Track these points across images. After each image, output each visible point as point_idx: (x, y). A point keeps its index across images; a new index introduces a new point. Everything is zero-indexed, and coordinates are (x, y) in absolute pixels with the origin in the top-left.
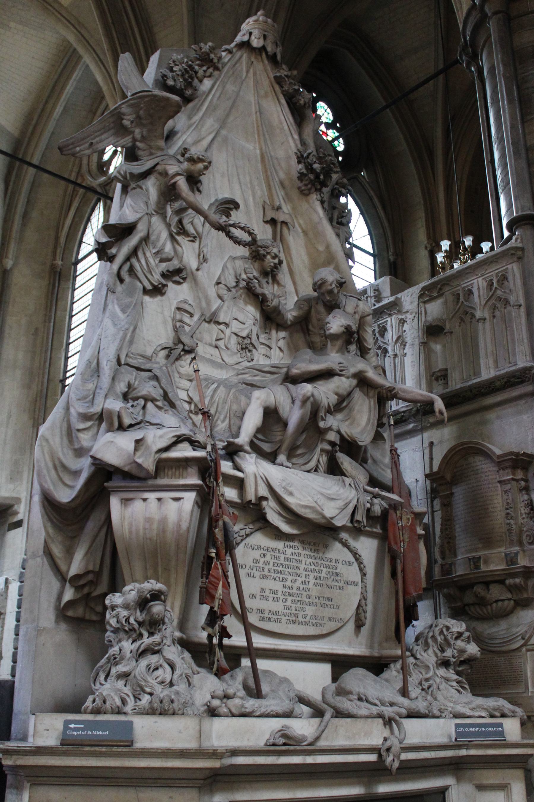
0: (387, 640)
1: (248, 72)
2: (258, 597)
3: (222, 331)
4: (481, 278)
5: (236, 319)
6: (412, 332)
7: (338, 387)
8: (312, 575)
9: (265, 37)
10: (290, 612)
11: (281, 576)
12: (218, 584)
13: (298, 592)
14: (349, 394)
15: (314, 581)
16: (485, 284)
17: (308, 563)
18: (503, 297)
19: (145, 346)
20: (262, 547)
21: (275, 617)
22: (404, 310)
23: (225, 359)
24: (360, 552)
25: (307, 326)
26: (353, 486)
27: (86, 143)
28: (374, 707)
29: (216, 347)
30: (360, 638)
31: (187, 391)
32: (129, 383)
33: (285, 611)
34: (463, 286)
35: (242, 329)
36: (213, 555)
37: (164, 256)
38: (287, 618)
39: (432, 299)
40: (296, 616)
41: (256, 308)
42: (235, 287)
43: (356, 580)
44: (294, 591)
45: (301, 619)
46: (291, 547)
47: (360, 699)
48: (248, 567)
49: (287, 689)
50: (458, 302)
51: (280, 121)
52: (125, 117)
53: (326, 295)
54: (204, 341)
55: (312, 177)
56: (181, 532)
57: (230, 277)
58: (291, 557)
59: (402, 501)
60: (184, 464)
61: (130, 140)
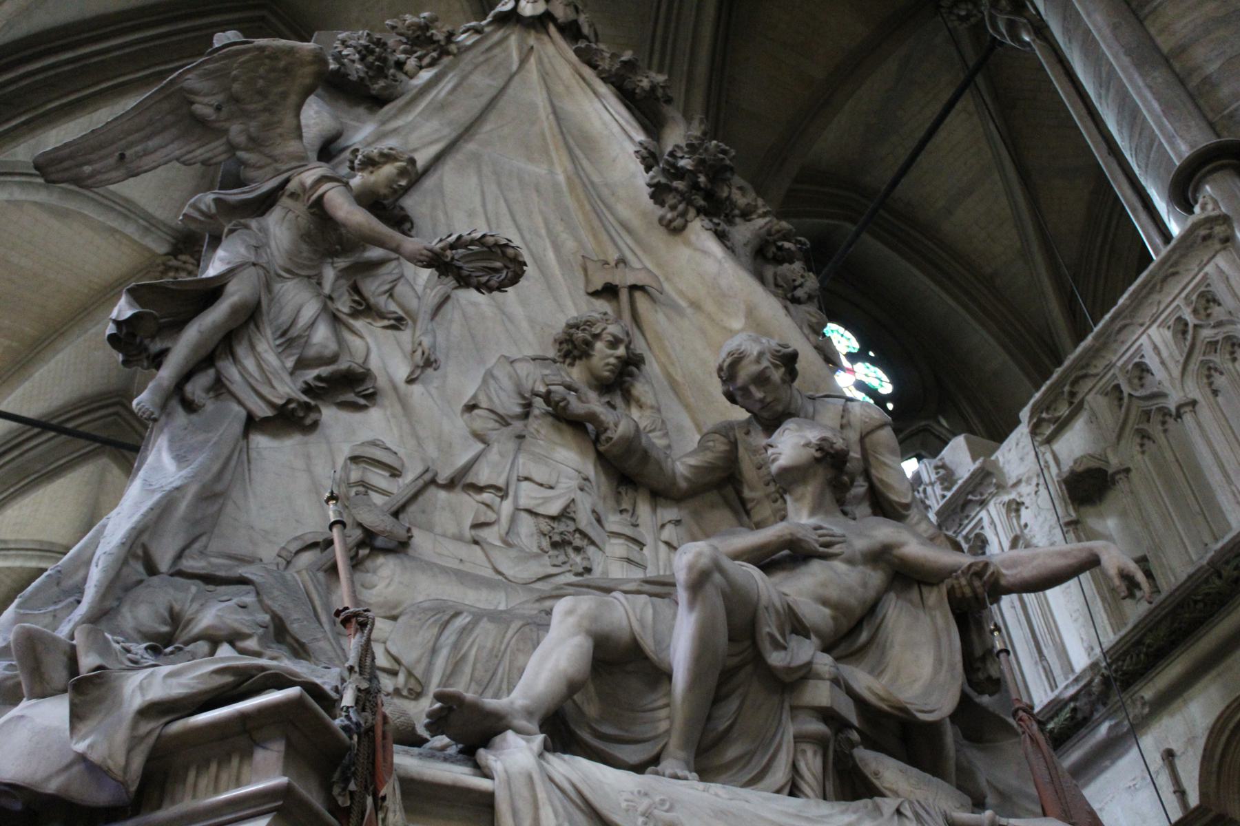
1: (523, 62)
3: (487, 506)
4: (1155, 326)
5: (527, 479)
6: (1041, 519)
16: (1168, 334)
18: (1220, 337)
22: (1011, 483)
25: (739, 493)
26: (908, 813)
29: (476, 542)
31: (385, 643)
34: (1119, 364)
35: (546, 500)
37: (311, 352)
39: (1062, 425)
41: (582, 453)
50: (1121, 399)
51: (604, 124)
53: (753, 389)
54: (438, 529)
55: (679, 184)
57: (502, 394)
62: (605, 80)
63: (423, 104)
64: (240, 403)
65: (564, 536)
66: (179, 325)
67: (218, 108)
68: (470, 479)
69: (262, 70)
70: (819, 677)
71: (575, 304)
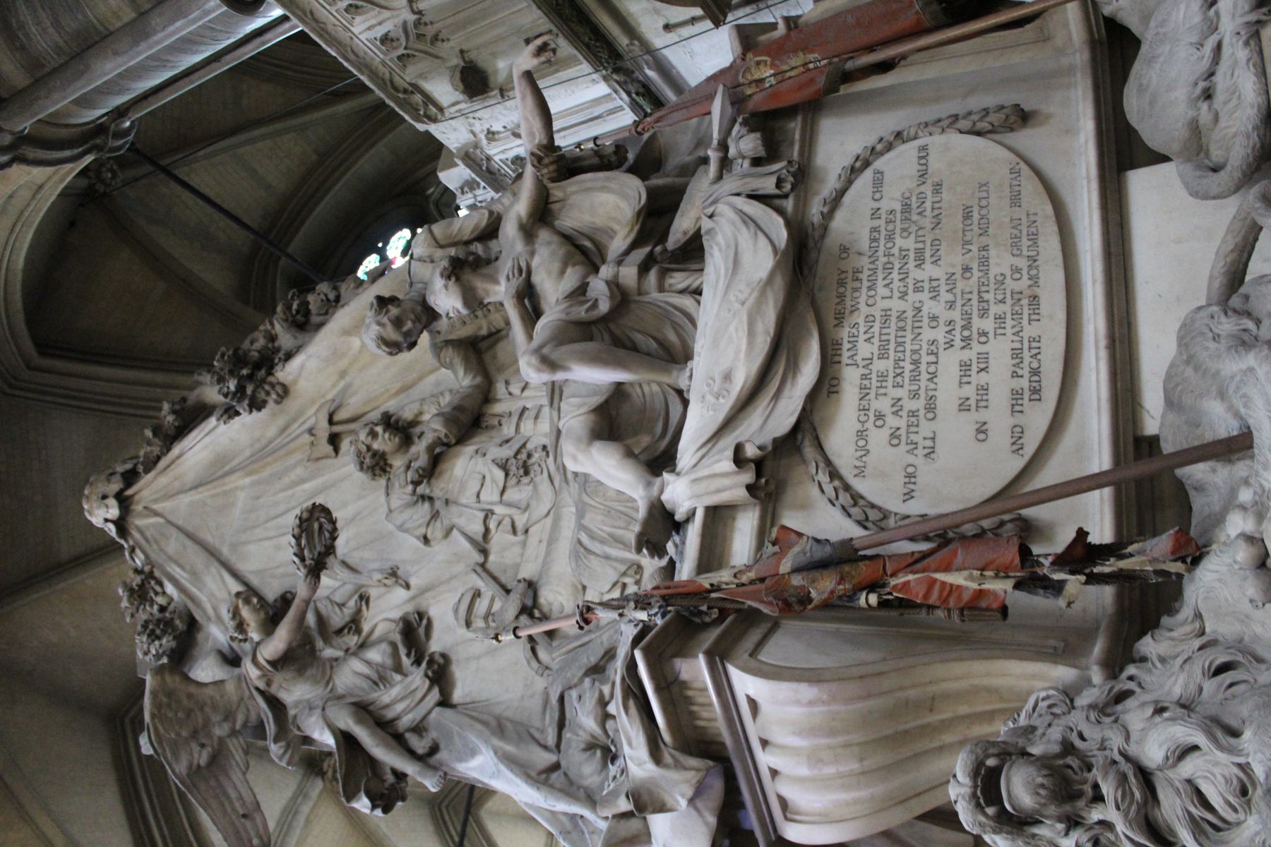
0: (1046, 39)
1: (156, 514)
2: (983, 415)
3: (499, 524)
5: (478, 496)
7: (549, 273)
8: (916, 274)
9: (104, 497)
10: (1009, 316)
11: (925, 359)
12: (943, 583)
13: (959, 303)
14: (567, 238)
15: (928, 266)
16: (358, 19)
17: (886, 292)
19: (532, 696)
20: (859, 426)
21: (1026, 355)
23: (545, 512)
24: (848, 161)
27: (245, 827)
28: (1226, 51)
29: (527, 531)
30: (1052, 109)
32: (585, 750)
33: (1009, 331)
35: (493, 481)
36: (873, 599)
37: (389, 662)
38: (1025, 322)
39: (429, 99)
40: (1017, 296)
41: (457, 456)
42: (432, 504)
43: (915, 153)
44: (956, 315)
45: (1025, 282)
46: (854, 344)
47: (1208, 95)
48: (911, 459)
49: (1212, 345)
50: (408, 56)
52: (195, 762)
53: (405, 329)
54: (518, 560)
56: (825, 697)
58: (876, 340)
59: (721, 88)
60: (675, 689)
61: (234, 740)
62: (169, 450)
63: (193, 590)
64: (429, 712)
65: (520, 466)
66: (373, 763)
67: (203, 746)
68: (479, 538)
69: (170, 715)
70: (616, 276)
71: (344, 466)
